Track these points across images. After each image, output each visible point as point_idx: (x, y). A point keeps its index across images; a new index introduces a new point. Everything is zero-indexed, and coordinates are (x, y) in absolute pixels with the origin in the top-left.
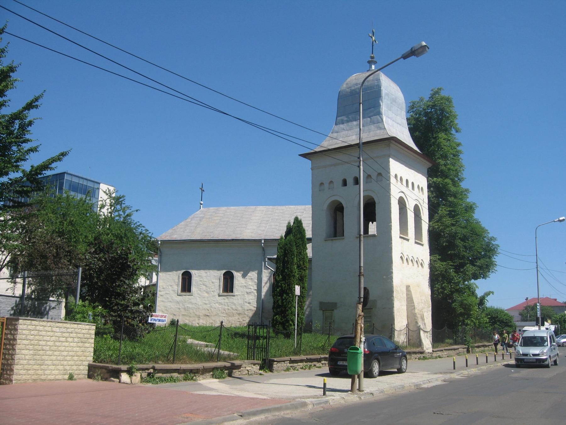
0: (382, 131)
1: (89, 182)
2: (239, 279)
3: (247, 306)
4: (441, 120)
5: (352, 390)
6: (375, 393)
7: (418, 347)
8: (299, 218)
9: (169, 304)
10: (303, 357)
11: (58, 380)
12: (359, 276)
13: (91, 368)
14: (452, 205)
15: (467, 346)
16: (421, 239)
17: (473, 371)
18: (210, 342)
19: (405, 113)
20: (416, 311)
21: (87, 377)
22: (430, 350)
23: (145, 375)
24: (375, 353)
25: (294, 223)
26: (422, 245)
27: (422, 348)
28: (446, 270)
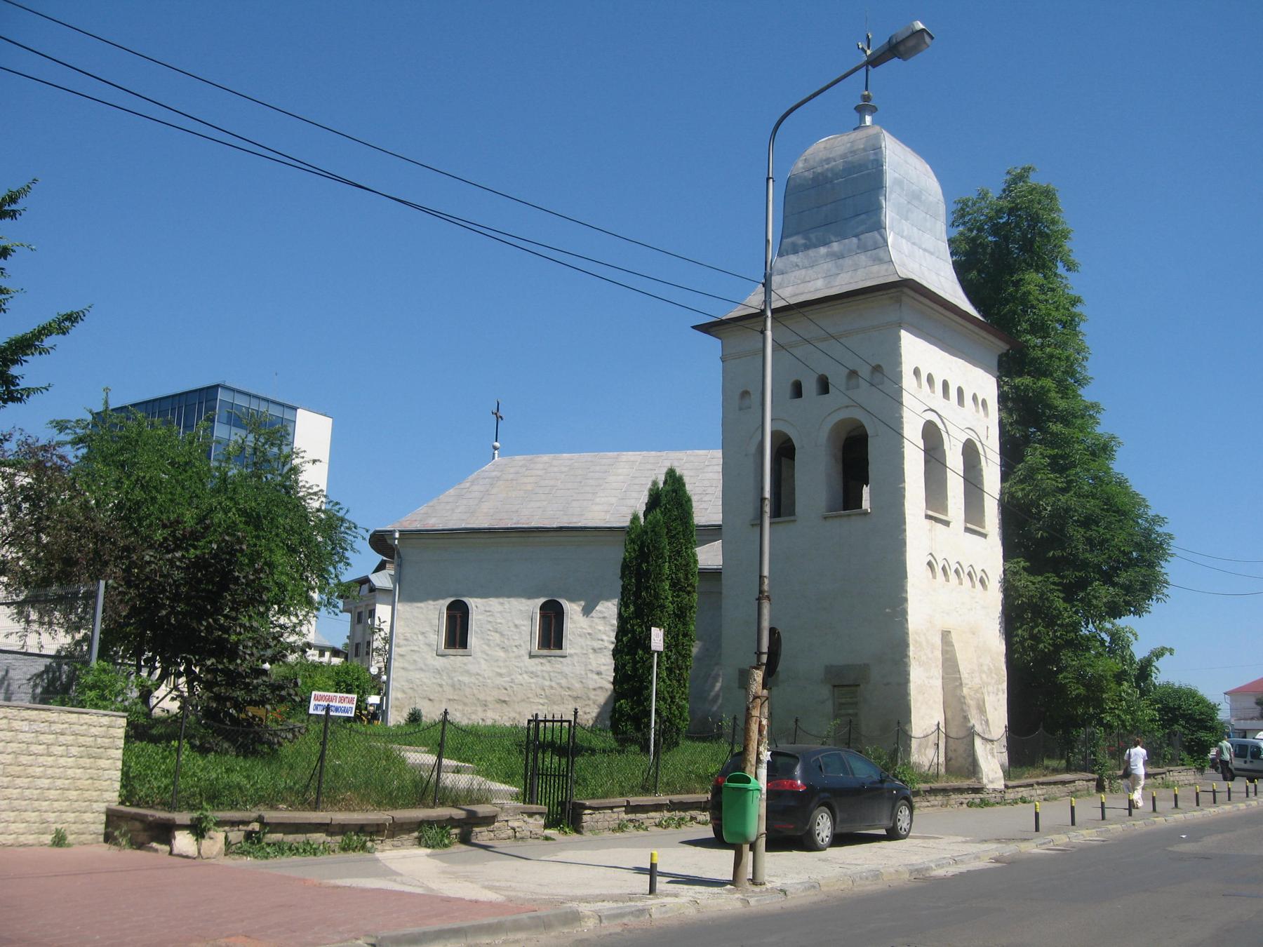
0: (884, 267)
1: (271, 405)
2: (575, 617)
3: (593, 680)
4: (1032, 241)
5: (734, 882)
6: (790, 890)
7: (968, 778)
8: (678, 472)
9: (418, 675)
10: (663, 798)
11: (25, 845)
12: (759, 599)
13: (113, 818)
14: (1054, 441)
15: (1096, 776)
16: (981, 523)
17: (1085, 836)
18: (469, 761)
19: (944, 227)
20: (965, 691)
21: (101, 838)
22: (1000, 784)
23: (236, 835)
24: (824, 790)
25: (665, 483)
26: (984, 536)
27: (979, 780)
28: (1042, 594)
